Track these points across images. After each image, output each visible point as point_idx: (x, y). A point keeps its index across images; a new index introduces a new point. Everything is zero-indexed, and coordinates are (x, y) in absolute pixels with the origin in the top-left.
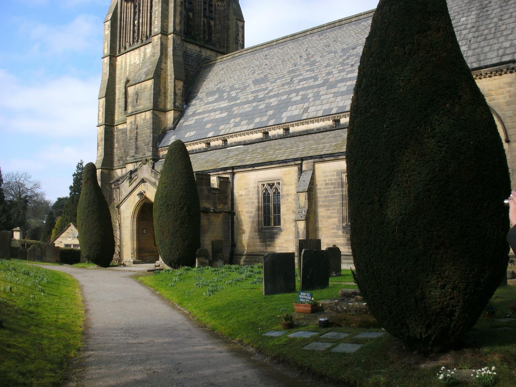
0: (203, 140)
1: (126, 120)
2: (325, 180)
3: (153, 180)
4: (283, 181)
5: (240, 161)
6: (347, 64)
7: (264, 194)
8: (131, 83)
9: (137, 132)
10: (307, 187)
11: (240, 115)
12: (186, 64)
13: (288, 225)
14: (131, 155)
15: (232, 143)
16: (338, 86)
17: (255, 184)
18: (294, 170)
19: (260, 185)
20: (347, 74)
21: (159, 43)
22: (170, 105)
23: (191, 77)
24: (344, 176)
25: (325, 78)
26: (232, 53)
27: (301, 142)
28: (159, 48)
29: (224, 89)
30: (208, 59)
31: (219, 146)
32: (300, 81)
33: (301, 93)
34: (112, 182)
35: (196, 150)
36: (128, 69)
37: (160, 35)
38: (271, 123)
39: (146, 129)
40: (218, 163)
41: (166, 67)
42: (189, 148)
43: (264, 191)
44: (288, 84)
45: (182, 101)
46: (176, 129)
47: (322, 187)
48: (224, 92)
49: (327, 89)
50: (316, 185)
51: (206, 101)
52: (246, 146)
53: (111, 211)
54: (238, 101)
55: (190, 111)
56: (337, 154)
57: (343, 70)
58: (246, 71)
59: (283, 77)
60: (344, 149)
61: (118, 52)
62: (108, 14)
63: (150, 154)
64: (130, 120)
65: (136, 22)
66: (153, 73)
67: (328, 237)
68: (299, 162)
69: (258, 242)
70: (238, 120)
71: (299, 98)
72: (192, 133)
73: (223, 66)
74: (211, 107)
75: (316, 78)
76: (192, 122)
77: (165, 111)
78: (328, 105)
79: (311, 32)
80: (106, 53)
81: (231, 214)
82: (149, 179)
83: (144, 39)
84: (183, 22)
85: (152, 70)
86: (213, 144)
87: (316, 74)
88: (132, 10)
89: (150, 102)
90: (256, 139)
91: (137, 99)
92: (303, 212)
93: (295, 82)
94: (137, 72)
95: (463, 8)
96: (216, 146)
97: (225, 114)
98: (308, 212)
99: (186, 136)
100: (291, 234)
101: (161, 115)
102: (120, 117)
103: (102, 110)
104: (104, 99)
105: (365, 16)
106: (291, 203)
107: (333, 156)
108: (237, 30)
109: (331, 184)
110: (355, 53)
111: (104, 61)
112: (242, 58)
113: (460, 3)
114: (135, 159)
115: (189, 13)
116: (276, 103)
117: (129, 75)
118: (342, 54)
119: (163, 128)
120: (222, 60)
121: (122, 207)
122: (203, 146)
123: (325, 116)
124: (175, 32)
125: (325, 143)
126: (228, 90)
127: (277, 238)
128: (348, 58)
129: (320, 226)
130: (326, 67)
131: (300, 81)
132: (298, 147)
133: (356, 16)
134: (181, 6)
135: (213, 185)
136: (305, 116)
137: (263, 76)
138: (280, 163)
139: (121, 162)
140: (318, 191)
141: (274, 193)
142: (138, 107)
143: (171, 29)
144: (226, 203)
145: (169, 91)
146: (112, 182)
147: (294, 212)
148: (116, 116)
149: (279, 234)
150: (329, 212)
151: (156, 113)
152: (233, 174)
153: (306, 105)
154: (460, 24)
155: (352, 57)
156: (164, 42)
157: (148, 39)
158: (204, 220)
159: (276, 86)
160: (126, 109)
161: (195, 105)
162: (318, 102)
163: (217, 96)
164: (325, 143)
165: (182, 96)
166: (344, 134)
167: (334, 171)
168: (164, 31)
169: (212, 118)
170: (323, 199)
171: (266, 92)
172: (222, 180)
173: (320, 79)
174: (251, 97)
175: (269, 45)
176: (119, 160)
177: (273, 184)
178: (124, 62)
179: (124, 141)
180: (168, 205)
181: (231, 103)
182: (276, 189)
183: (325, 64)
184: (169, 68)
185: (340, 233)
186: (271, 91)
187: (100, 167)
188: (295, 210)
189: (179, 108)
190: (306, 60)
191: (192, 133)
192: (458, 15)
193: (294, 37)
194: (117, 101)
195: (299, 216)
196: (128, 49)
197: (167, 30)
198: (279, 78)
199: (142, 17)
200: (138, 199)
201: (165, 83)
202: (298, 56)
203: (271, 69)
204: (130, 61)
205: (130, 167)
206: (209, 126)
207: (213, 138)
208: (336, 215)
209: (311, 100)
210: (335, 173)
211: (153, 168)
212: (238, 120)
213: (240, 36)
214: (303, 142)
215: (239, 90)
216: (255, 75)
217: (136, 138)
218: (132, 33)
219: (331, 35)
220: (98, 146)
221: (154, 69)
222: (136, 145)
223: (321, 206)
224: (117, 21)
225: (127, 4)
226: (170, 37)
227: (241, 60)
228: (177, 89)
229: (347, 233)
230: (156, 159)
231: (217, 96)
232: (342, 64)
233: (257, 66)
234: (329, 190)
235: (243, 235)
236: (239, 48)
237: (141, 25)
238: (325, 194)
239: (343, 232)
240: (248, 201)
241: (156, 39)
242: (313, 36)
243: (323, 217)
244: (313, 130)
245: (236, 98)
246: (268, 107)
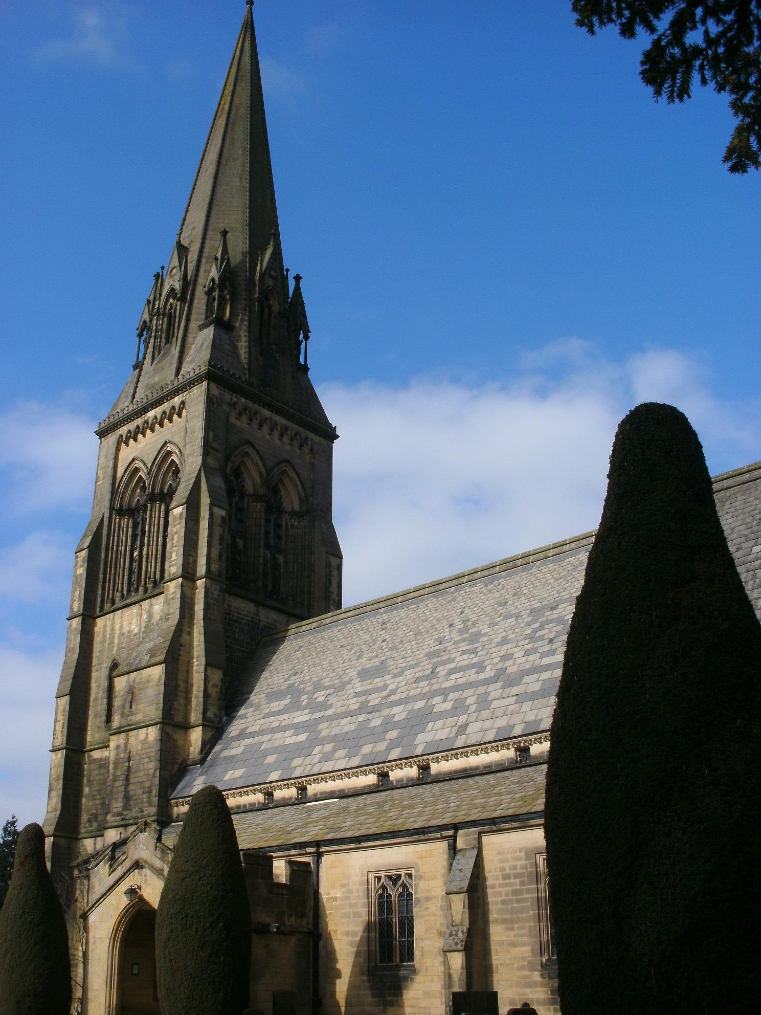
0: (258, 787)
1: (109, 741)
2: (503, 869)
3: (158, 863)
4: (418, 871)
5: (333, 829)
6: (542, 638)
7: (381, 896)
8: (122, 668)
9: (129, 767)
10: (467, 882)
11: (334, 739)
12: (229, 637)
13: (428, 962)
14: (114, 810)
15: (316, 794)
16: (524, 681)
17: (362, 876)
18: (440, 848)
19: (372, 877)
20: (541, 658)
21: (178, 595)
22: (195, 716)
23: (238, 663)
24: (541, 859)
25: (499, 666)
26: (318, 618)
27: (454, 792)
28: (177, 604)
29: (302, 686)
30: (272, 629)
31: (290, 798)
32: (451, 672)
33: (452, 696)
34: (74, 863)
35: (245, 806)
36: (116, 641)
37: (180, 580)
38: (395, 754)
39: (146, 760)
40: (290, 833)
41: (191, 641)
42: (231, 802)
43: (381, 891)
44: (427, 678)
45: (220, 709)
46: (207, 764)
47: (497, 883)
48: (301, 692)
49: (503, 688)
50: (485, 879)
51: (267, 711)
52: (344, 800)
53: (68, 925)
54: (330, 712)
55: (234, 729)
56: (525, 817)
57: (534, 651)
58: (344, 652)
59: (417, 665)
60: (540, 804)
61: (98, 609)
62: (85, 536)
63: (153, 810)
64: (114, 741)
65: (136, 554)
66: (165, 652)
67: (511, 986)
68: (451, 833)
69: (367, 997)
70: (328, 748)
71: (448, 705)
72: (239, 773)
73: (300, 642)
74: (275, 722)
75: (480, 667)
76: (239, 751)
77: (186, 727)
78: (506, 718)
79: (470, 577)
80: (76, 609)
81: (314, 939)
82: (149, 861)
83: (150, 586)
84: (224, 557)
85: (163, 646)
86: (278, 794)
87: (481, 659)
88: (130, 530)
89: (157, 709)
90: (365, 787)
91: (131, 702)
92: (460, 935)
93: (440, 675)
94: (133, 649)
95: (755, 528)
96: (284, 799)
97: (302, 737)
98: (470, 933)
99: (227, 778)
100: (436, 979)
101: (178, 736)
102: (97, 736)
103: (63, 719)
104: (67, 698)
105: (573, 545)
106: (434, 915)
107: (519, 821)
108: (329, 574)
109: (515, 876)
110: (556, 616)
111: (71, 625)
112: (336, 626)
113: (749, 520)
114: (123, 820)
115: (238, 540)
116: (404, 715)
117: (117, 655)
118: (530, 619)
119: (180, 761)
120: (298, 630)
121: (93, 918)
122: (259, 797)
123: (501, 741)
124: (209, 575)
125: (500, 794)
126: (310, 688)
127: (407, 988)
128: (542, 627)
129: (494, 962)
130: (499, 644)
131: (451, 672)
132: (447, 802)
133: (555, 547)
134: (221, 526)
135: (278, 876)
136: (460, 742)
137: (378, 663)
138: (412, 835)
139: (95, 825)
140: (489, 891)
141: (401, 895)
142: (133, 718)
143: (201, 569)
144: (303, 915)
145: (195, 689)
146: (74, 863)
147: (441, 934)
148: (89, 733)
149: (412, 980)
150: (513, 933)
151: (169, 729)
152: (319, 856)
153: (463, 719)
154: (751, 557)
155: (551, 625)
156: (188, 592)
157: (156, 586)
158: (258, 949)
159: (404, 683)
160: (109, 719)
161: (244, 716)
162: (485, 714)
163: (287, 701)
164: (500, 794)
165: (219, 699)
166: (540, 775)
167: (521, 850)
168: (188, 573)
169: (277, 744)
170: (500, 906)
171: (384, 693)
172: (295, 868)
173: (488, 668)
174: (354, 704)
175: (391, 602)
176: (89, 821)
177: (399, 876)
178: (108, 629)
179: (103, 782)
180: (187, 916)
181: (315, 716)
182: (404, 886)
183: (499, 640)
184: (195, 643)
185: (536, 976)
186: (394, 692)
187: (52, 832)
188: (443, 929)
189: (213, 722)
190: (461, 632)
191: (239, 773)
192: (747, 540)
193: (437, 588)
194: (91, 703)
195: (450, 941)
196: (118, 604)
197: (195, 570)
198: (410, 667)
199: (148, 545)
200: (125, 901)
201: (188, 671)
202: (445, 623)
203: (393, 648)
204: (121, 628)
205: (112, 836)
206: (271, 759)
207: (279, 784)
208: (526, 939)
209: (473, 708)
210: (523, 854)
211: (159, 839)
212: (328, 748)
213: (334, 584)
214: (457, 792)
215: (332, 690)
216: (363, 660)
217: (127, 779)
218: (126, 573)
219: (509, 582)
220: (50, 791)
221: (167, 644)
222: (127, 792)
223: (497, 921)
224: (100, 550)
225: (120, 520)
226: (200, 583)
227: (334, 632)
228: (210, 685)
229: (550, 978)
230: (164, 820)
231: (287, 701)
232: (532, 638)
233: (366, 642)
234: (510, 889)
235: (338, 981)
236: (332, 607)
237: (144, 560)
238: (504, 898)
239: (542, 976)
240: (347, 910)
241: (173, 588)
242: (474, 585)
243: (501, 943)
244: (477, 768)
245: (324, 706)
246: (389, 723)
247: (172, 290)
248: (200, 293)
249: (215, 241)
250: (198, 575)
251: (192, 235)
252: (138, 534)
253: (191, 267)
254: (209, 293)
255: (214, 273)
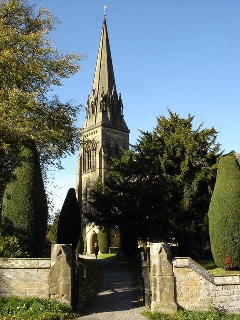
124: (105, 168)
143: (103, 167)
241: (98, 171)
247: (93, 102)
248: (99, 103)
249: (101, 90)
250: (95, 258)
251: (96, 87)
252: (90, 156)
253: (96, 95)
254: (101, 103)
255: (101, 99)
